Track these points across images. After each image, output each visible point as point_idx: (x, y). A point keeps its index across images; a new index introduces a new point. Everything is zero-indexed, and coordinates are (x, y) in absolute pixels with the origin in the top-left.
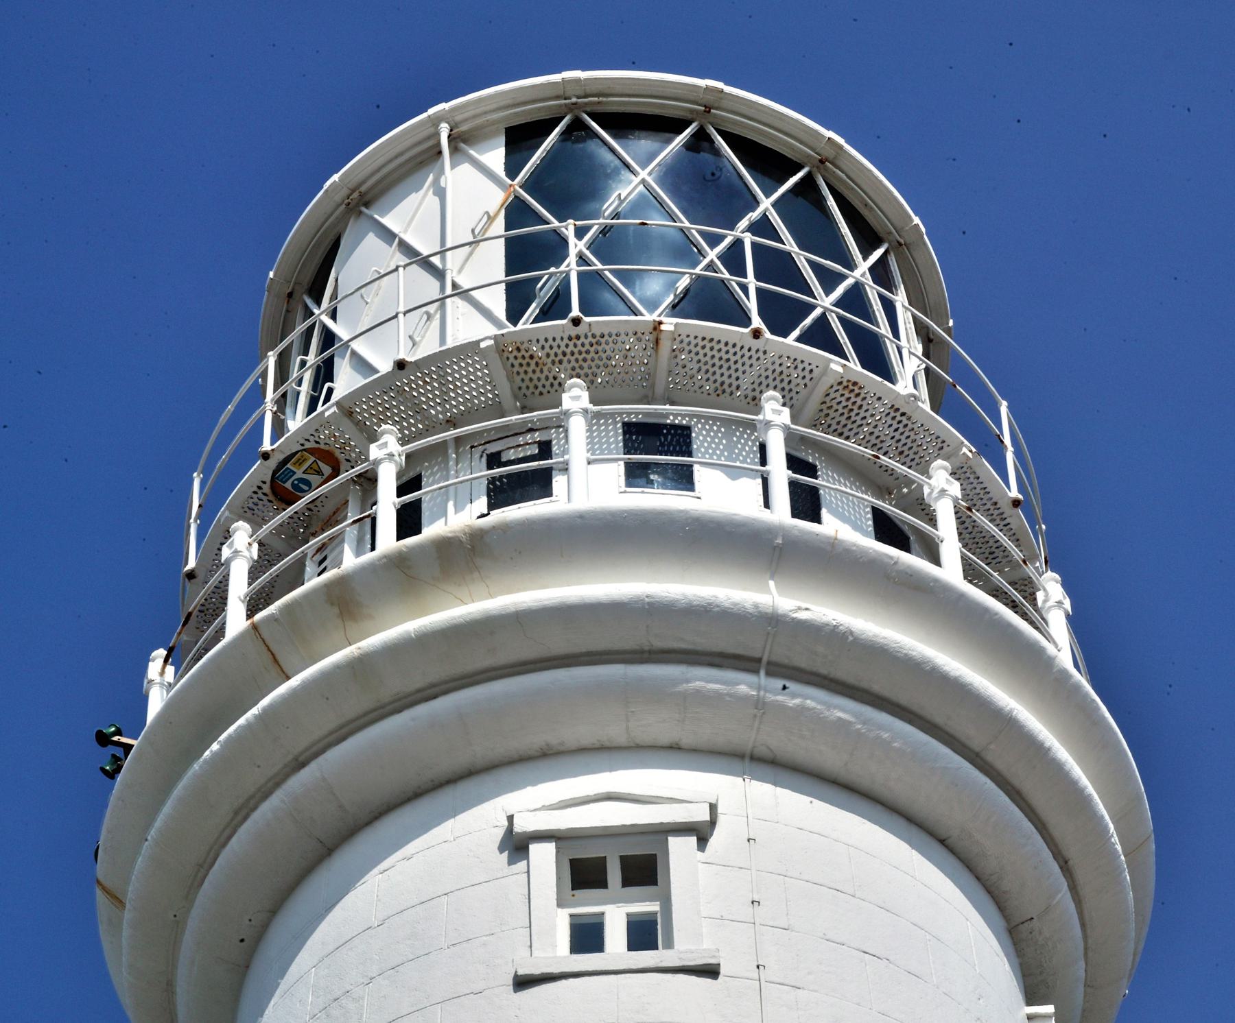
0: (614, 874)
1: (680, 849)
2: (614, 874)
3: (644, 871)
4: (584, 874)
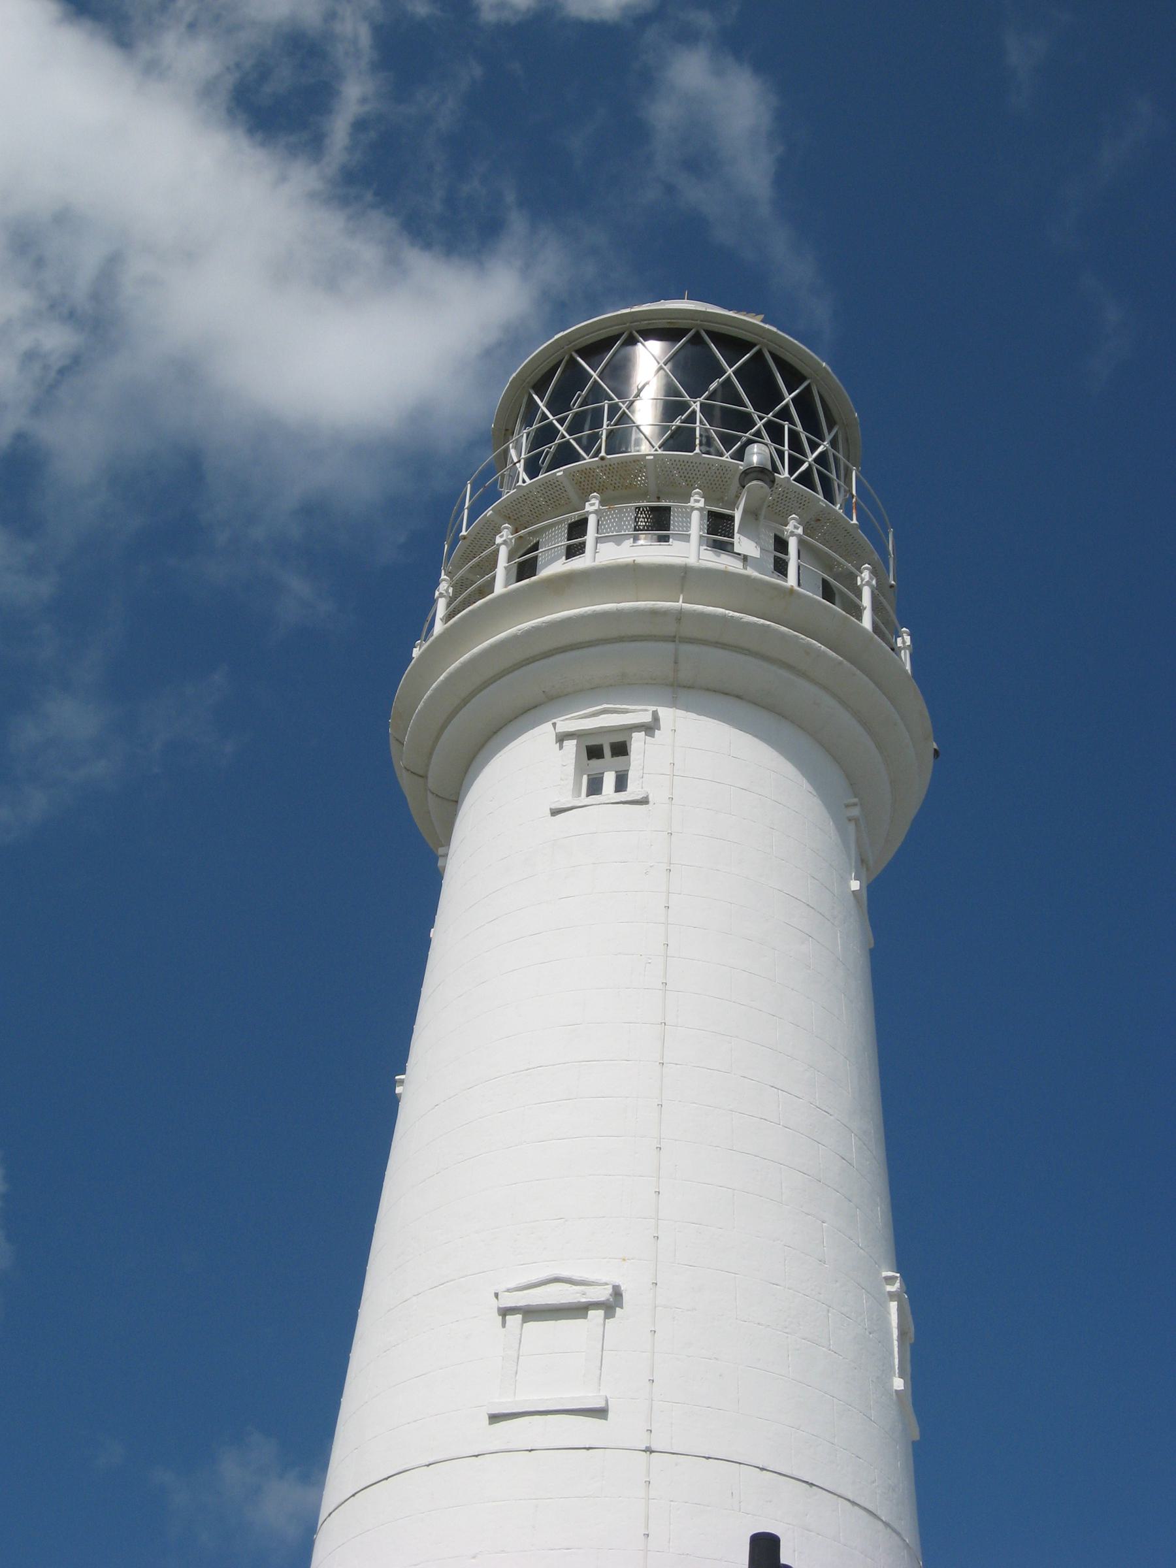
0: (607, 751)
1: (638, 741)
2: (607, 751)
3: (621, 749)
4: (594, 752)
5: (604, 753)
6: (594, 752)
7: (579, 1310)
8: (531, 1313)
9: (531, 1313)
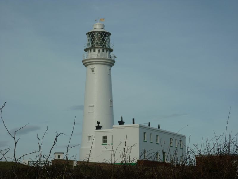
3: (93, 69)
8: (90, 107)
9: (90, 107)
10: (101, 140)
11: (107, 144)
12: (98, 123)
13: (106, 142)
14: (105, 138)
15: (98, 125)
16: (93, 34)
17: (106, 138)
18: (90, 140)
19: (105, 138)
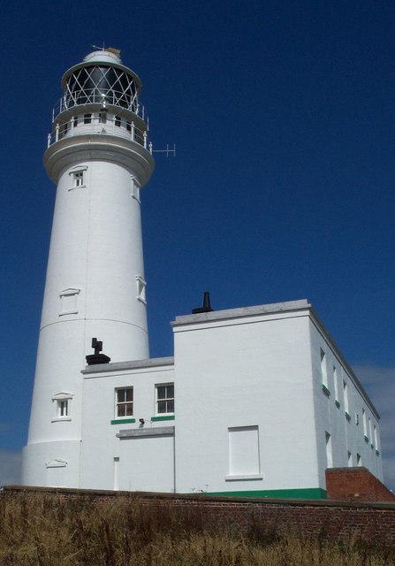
3: (81, 175)
5: (79, 175)
6: (77, 175)
7: (74, 294)
10: (113, 399)
11: (133, 421)
12: (97, 345)
13: (130, 411)
14: (125, 394)
15: (97, 351)
16: (83, 72)
17: (130, 397)
18: (62, 414)
19: (125, 394)
